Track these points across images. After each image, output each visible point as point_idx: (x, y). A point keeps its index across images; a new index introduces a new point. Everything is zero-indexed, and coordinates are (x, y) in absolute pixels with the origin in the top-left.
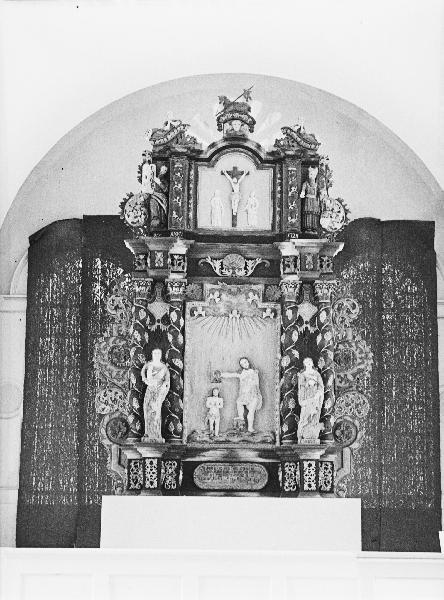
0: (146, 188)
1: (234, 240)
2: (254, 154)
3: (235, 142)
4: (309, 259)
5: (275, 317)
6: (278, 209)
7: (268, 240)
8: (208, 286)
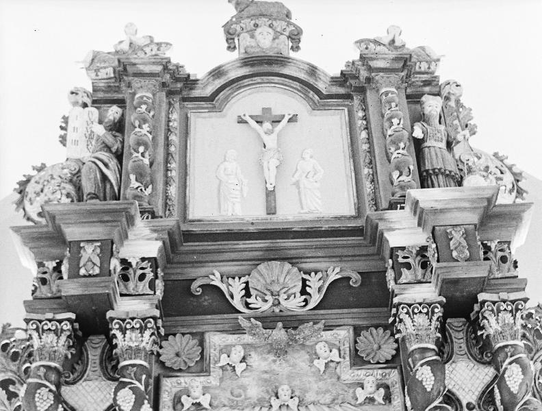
0: (81, 151)
1: (274, 241)
2: (307, 86)
3: (264, 67)
4: (457, 236)
5: (388, 398)
6: (366, 171)
7: (362, 235)
8: (215, 340)
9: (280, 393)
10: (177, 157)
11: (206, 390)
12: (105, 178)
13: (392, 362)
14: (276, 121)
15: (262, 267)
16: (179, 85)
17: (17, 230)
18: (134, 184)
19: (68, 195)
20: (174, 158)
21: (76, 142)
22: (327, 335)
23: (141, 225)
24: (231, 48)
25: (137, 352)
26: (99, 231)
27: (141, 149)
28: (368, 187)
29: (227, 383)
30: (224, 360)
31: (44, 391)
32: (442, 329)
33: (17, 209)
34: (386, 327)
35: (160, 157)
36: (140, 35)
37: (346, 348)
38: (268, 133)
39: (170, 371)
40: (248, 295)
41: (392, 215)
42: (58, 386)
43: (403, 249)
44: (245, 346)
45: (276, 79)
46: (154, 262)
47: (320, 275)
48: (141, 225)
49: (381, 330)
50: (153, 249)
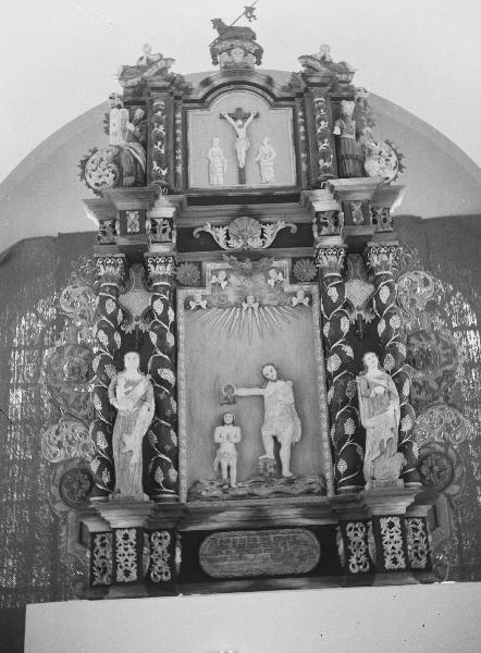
1: (246, 203)
2: (266, 89)
3: (237, 79)
4: (357, 208)
8: (209, 266)
9: (248, 300)
10: (181, 145)
11: (204, 297)
12: (136, 161)
13: (313, 280)
14: (245, 118)
15: (236, 221)
16: (181, 93)
17: (87, 202)
18: (156, 167)
19: (113, 172)
20: (179, 145)
21: (115, 134)
22: (276, 264)
23: (163, 200)
24: (215, 63)
25: (164, 277)
27: (159, 143)
28: (304, 167)
29: (217, 293)
32: (345, 263)
34: (311, 259)
35: (171, 146)
36: (153, 53)
37: (287, 271)
38: (240, 127)
39: (182, 285)
40: (228, 238)
41: (318, 192)
43: (323, 212)
44: (227, 270)
45: (247, 87)
46: (171, 220)
48: (163, 200)
49: (308, 261)
50: (169, 212)
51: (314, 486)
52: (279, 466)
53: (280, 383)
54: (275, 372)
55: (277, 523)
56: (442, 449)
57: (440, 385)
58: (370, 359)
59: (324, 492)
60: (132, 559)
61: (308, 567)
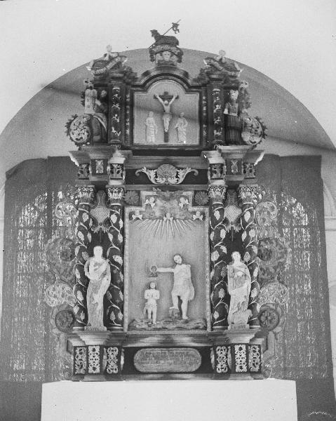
4: (234, 164)
5: (204, 218)
8: (144, 193)
11: (141, 212)
26: (102, 156)
30: (147, 202)
31: (84, 214)
33: (67, 135)
34: (206, 192)
37: (191, 198)
39: (128, 205)
42: (89, 211)
45: (171, 77)
46: (122, 165)
47: (183, 170)
51: (200, 325)
52: (181, 313)
53: (184, 266)
54: (181, 260)
55: (178, 344)
56: (274, 307)
57: (276, 270)
58: (236, 255)
59: (205, 328)
60: (244, 360)
61: (194, 368)
